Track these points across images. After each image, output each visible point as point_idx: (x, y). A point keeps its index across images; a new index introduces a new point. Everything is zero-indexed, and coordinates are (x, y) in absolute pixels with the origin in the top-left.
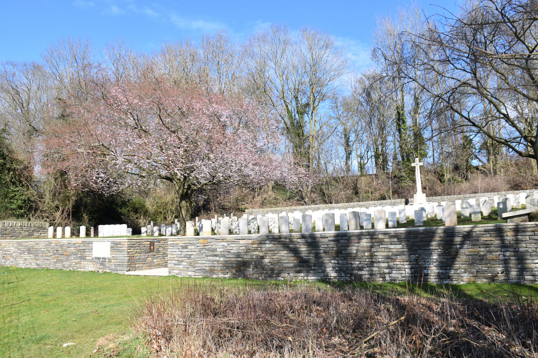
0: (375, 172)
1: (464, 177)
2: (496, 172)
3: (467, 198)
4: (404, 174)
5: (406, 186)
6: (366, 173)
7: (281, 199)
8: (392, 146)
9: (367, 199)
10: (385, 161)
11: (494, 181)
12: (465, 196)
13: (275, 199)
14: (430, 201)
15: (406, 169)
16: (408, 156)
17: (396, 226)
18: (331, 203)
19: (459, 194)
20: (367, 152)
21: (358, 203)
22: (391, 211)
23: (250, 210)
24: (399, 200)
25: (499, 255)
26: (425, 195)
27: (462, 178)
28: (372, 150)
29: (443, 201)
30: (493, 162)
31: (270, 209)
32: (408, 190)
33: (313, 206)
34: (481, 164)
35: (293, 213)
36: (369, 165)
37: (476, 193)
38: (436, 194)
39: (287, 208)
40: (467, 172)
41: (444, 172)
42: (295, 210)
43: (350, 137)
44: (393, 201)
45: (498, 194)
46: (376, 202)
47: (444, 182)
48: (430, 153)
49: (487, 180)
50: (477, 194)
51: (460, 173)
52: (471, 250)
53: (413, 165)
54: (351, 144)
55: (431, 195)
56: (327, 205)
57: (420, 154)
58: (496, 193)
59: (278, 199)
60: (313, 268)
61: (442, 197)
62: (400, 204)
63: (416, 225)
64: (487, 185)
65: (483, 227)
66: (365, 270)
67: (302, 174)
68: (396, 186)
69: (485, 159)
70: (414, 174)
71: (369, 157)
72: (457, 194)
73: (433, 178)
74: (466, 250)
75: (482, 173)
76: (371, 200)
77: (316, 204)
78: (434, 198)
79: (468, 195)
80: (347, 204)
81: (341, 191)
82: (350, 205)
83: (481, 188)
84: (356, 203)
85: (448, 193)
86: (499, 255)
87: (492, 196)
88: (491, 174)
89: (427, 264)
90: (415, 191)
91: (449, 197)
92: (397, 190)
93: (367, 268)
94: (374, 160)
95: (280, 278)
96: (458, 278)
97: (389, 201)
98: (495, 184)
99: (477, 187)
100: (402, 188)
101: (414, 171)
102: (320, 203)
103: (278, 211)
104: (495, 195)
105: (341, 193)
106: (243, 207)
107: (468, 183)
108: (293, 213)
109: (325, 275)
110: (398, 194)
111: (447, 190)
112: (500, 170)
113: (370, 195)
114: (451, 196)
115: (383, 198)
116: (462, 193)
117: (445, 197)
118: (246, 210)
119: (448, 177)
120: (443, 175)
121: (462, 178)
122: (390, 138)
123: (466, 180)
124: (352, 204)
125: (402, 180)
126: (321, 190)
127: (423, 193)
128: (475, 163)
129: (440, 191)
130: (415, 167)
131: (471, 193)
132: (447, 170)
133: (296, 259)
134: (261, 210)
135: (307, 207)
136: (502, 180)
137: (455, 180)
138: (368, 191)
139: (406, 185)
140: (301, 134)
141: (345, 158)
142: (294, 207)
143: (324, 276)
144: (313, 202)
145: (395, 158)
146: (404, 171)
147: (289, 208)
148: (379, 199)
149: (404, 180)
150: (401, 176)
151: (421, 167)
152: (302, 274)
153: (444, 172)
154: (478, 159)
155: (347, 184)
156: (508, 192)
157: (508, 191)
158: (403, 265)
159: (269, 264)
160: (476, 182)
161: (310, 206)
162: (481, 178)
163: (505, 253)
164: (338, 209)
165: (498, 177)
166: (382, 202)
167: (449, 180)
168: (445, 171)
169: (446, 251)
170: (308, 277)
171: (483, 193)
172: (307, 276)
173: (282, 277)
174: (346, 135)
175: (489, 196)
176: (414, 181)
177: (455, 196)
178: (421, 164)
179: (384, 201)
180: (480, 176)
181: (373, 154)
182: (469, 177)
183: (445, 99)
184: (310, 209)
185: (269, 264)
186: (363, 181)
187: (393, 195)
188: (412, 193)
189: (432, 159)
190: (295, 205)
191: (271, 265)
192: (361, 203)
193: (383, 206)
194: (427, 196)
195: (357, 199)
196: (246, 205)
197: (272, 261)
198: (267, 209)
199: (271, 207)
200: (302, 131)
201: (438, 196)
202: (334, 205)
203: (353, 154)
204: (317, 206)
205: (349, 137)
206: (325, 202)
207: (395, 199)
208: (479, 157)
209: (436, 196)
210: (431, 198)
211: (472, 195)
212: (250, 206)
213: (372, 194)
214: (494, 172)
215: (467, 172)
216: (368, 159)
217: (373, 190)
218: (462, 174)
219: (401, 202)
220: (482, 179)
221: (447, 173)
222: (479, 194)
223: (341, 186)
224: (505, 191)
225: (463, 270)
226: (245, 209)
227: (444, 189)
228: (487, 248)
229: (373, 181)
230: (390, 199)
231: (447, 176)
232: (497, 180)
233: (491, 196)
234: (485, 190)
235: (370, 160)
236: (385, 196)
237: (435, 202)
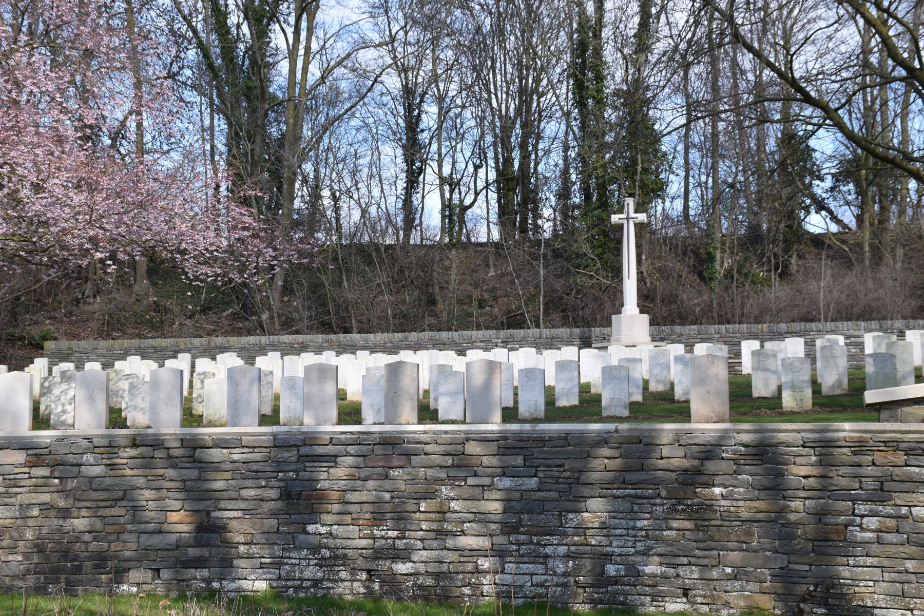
0: (496, 235)
1: (776, 269)
2: (880, 258)
3: (780, 334)
4: (586, 248)
5: (592, 287)
6: (468, 237)
7: (177, 309)
8: (556, 157)
9: (464, 323)
10: (531, 201)
11: (870, 284)
12: (775, 327)
13: (157, 308)
14: (662, 340)
15: (594, 232)
16: (602, 187)
17: (541, 414)
18: (347, 331)
19: (758, 320)
20: (477, 168)
21: (433, 334)
22: (363, 407)
23: (64, 344)
24: (564, 332)
25: (846, 526)
26: (646, 318)
27: (769, 271)
28: (491, 163)
29: (703, 341)
30: (872, 225)
31: (135, 342)
32: (595, 299)
33: (286, 338)
34: (834, 228)
35: (214, 359)
36: (479, 212)
37: (812, 321)
38: (683, 318)
39: (197, 341)
40: (786, 251)
41: (715, 248)
42: (224, 349)
43: (424, 116)
44: (546, 332)
45: (881, 329)
46: (492, 333)
47: (711, 279)
48: (675, 186)
49: (847, 281)
50: (813, 325)
51: (763, 255)
52: (756, 504)
53: (615, 218)
54: (424, 137)
55: (669, 320)
56: (332, 336)
57: (640, 187)
58: (875, 325)
59: (166, 310)
60: (242, 548)
61: (703, 327)
62: (569, 343)
63: (605, 414)
64: (848, 296)
65: (799, 431)
66: (415, 559)
67: (244, 229)
68: (559, 285)
69: (848, 213)
70: (618, 251)
71: (480, 187)
72: (752, 320)
73: (678, 266)
74: (741, 503)
75: (833, 258)
76: (479, 327)
77: (297, 332)
78: (678, 329)
79: (783, 326)
80: (399, 336)
81: (381, 293)
82: (406, 339)
83: (827, 305)
84: (428, 335)
85: (720, 316)
86: (846, 526)
87: (862, 332)
88: (863, 261)
89: (615, 543)
90: (617, 303)
91: (723, 328)
92: (561, 298)
93: (424, 553)
94: (493, 196)
95: (125, 587)
96: (712, 596)
97: (533, 332)
98: (873, 295)
99: (816, 302)
100: (578, 292)
101: (620, 242)
102: (311, 329)
103: (165, 349)
104: (871, 331)
105: (380, 298)
106: (35, 332)
107: (787, 288)
108: (214, 359)
109: (283, 573)
110: (564, 311)
111: (719, 305)
112: (893, 250)
113: (474, 310)
114: (730, 327)
115: (514, 321)
116: (768, 317)
117: (712, 328)
118: (49, 345)
119: (726, 265)
120: (711, 258)
121: (769, 271)
122: (552, 128)
123: (780, 276)
124: (413, 336)
125: (578, 267)
126: (315, 287)
127: (641, 312)
128: (816, 223)
129: (698, 309)
130: (620, 227)
131: (793, 321)
132: (723, 243)
133: (188, 520)
134: (103, 344)
135: (264, 340)
136: (897, 284)
137: (746, 275)
138: (470, 297)
139: (589, 282)
140: (258, 92)
141: (401, 184)
142: (219, 340)
143: (279, 578)
144: (288, 326)
145: (564, 194)
146: (587, 240)
147: (204, 340)
148: (502, 326)
149: (586, 267)
150: (577, 255)
151: (640, 227)
152: (205, 573)
153: (715, 248)
154: (830, 212)
155: (401, 271)
156: (912, 322)
157: (913, 318)
158: (538, 544)
159: (87, 537)
160: (812, 287)
161: (274, 338)
162: (829, 272)
163: (865, 520)
164: (368, 352)
165: (884, 272)
166: (512, 336)
167: (729, 274)
168: (718, 245)
169: (679, 504)
170: (225, 583)
171: (833, 320)
172: (221, 580)
173: (133, 584)
174: (409, 108)
175: (852, 332)
176: (617, 272)
177: (744, 327)
178: (642, 217)
179: (519, 333)
180: (826, 268)
181: (492, 175)
182: (794, 268)
183: (309, 75)
184: (274, 347)
185: (87, 537)
186: (454, 265)
187: (546, 312)
188: (608, 307)
189: (679, 205)
190: (225, 334)
191: (95, 539)
192: (444, 335)
193: (510, 350)
194: (652, 323)
195: (433, 321)
196: (50, 327)
197: (99, 525)
198: (126, 343)
199: (140, 336)
200: (261, 81)
201: (691, 324)
202: (355, 337)
203: (430, 175)
204: (300, 338)
205: (419, 115)
206: (326, 327)
207: (553, 327)
208: (832, 205)
209: (683, 324)
210: (666, 329)
211: (796, 326)
212: (63, 329)
213: (481, 306)
214: (873, 256)
215: (786, 251)
216: (477, 194)
217: (486, 296)
218: (769, 258)
219: (571, 336)
220: (833, 276)
221: (723, 251)
222: (820, 325)
223: (382, 278)
224: (904, 318)
225: (729, 570)
226: (45, 338)
227: (711, 305)
228: (807, 502)
229: (488, 266)
230: (538, 326)
231: (723, 263)
232: (880, 284)
233: (857, 333)
234: (839, 311)
235: (481, 197)
236: (522, 314)
237: (680, 342)
